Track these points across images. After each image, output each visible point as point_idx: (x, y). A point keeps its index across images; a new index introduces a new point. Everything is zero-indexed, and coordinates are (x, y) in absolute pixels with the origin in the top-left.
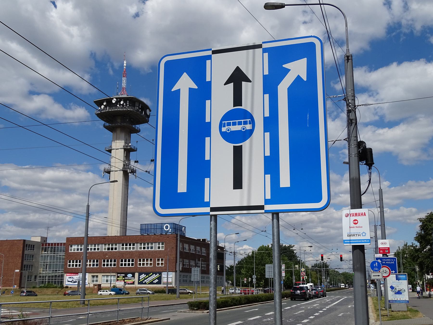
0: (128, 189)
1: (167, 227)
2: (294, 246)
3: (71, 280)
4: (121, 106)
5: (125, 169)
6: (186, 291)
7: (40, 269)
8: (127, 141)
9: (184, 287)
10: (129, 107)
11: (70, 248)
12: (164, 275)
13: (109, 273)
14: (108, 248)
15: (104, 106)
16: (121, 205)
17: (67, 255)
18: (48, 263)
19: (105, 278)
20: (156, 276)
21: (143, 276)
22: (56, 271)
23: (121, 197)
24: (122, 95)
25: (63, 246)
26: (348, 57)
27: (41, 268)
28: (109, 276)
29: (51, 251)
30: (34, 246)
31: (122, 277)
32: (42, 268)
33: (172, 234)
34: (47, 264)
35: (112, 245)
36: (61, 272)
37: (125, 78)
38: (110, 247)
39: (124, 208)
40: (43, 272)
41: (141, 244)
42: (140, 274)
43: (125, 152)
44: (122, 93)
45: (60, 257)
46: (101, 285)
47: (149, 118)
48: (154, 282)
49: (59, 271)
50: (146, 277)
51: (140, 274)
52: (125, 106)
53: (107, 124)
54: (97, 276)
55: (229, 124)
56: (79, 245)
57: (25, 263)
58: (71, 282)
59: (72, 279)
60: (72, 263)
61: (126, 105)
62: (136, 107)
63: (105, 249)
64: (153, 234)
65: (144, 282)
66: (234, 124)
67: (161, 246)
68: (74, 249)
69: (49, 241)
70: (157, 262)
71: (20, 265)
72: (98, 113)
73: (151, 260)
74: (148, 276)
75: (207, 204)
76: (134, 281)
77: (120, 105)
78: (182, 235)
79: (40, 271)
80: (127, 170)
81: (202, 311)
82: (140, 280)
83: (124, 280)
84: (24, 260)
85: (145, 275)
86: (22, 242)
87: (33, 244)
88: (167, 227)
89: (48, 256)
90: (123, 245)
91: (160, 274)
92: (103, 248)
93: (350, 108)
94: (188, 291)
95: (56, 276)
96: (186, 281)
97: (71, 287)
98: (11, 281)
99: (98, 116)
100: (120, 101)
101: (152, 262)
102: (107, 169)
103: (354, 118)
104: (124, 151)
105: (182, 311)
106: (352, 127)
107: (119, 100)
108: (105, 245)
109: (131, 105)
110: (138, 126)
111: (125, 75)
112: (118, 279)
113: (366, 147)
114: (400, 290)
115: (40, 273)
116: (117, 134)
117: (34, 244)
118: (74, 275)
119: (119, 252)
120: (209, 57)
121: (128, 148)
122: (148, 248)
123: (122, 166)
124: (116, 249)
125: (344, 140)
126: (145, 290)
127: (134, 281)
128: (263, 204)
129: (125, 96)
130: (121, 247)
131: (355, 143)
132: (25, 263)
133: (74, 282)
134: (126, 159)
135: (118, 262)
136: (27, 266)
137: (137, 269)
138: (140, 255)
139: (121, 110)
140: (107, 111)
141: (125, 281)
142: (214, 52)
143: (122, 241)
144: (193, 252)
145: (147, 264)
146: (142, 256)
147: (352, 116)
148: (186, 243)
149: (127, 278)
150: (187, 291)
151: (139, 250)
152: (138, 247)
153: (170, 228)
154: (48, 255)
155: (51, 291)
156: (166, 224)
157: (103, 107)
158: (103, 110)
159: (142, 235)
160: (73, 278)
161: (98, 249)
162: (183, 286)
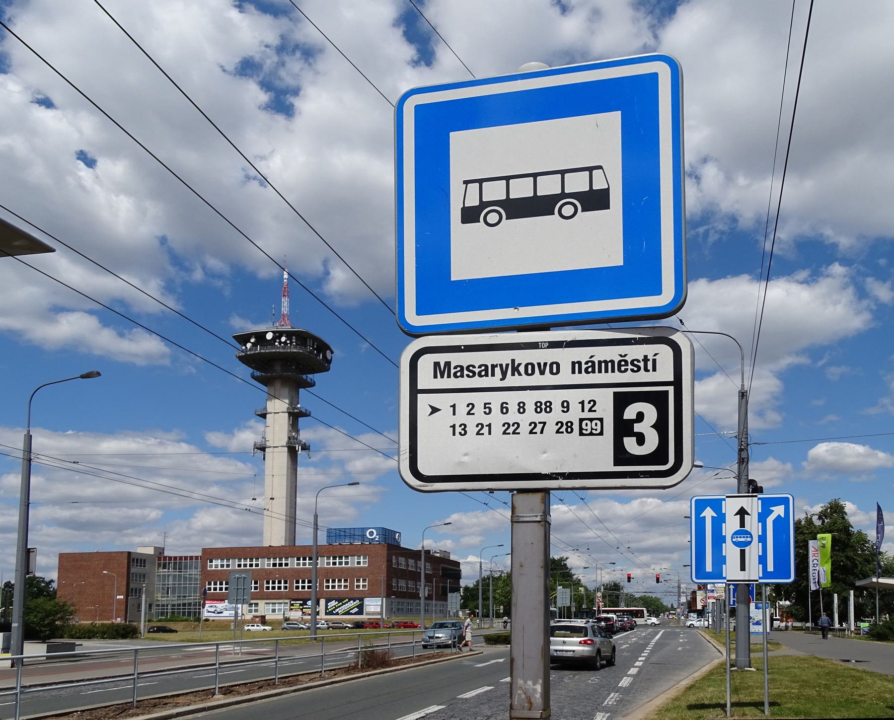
0: (296, 474)
1: (371, 534)
2: (567, 558)
3: (212, 609)
4: (282, 345)
5: (291, 444)
6: (341, 625)
7: (157, 594)
8: (293, 402)
9: (398, 618)
10: (295, 347)
11: (209, 564)
12: (367, 601)
13: (282, 599)
14: (273, 563)
15: (251, 344)
16: (24, 443)
17: (204, 573)
18: (170, 586)
19: (271, 607)
20: (355, 603)
21: (333, 603)
22: (185, 597)
23: (285, 488)
24: (283, 327)
25: (194, 561)
26: (743, 393)
27: (159, 593)
28: (277, 604)
29: (175, 568)
30: (145, 561)
31: (298, 605)
32: (160, 592)
33: (380, 543)
34: (168, 588)
35: (281, 559)
36: (193, 599)
37: (287, 299)
38: (278, 562)
39: (290, 504)
40: (162, 599)
41: (328, 558)
42: (328, 601)
43: (291, 417)
44: (283, 323)
45: (190, 576)
46: (264, 616)
47: (331, 365)
48: (351, 612)
49: (189, 596)
50: (339, 605)
51: (328, 601)
52: (289, 345)
53: (258, 374)
54: (256, 604)
55: (737, 537)
56: (224, 560)
57: (132, 586)
58: (214, 612)
59: (215, 609)
60: (214, 585)
61: (291, 343)
62: (308, 347)
63: (269, 565)
64: (349, 543)
65: (334, 612)
66: (740, 537)
67: (362, 560)
68: (216, 566)
69: (166, 554)
70: (356, 584)
71: (125, 588)
72: (241, 354)
73: (346, 581)
74: (341, 604)
75: (725, 578)
76: (319, 611)
77: (280, 343)
78: (395, 544)
79: (157, 597)
80: (294, 445)
81: (505, 646)
82: (328, 609)
83: (302, 609)
84: (131, 581)
85: (337, 602)
86: (126, 555)
87: (143, 558)
88: (371, 534)
89: (169, 575)
90: (298, 559)
91: (362, 600)
92: (266, 564)
93: (742, 447)
94: (345, 625)
95: (184, 605)
96: (411, 610)
97: (213, 620)
98: (111, 613)
99: (240, 360)
100: (280, 338)
101: (348, 584)
102: (259, 444)
103: (746, 456)
104: (289, 417)
105: (478, 645)
106: (744, 466)
107: (277, 335)
108: (269, 559)
109: (299, 343)
110: (310, 376)
111: (286, 294)
112: (292, 607)
113: (757, 485)
114: (759, 620)
115: (157, 600)
116: (275, 389)
117: (145, 558)
118: (218, 602)
119: (292, 570)
120: (724, 500)
121: (296, 411)
122: (341, 563)
123: (286, 439)
124: (286, 565)
125: (734, 478)
126: (296, 624)
127: (319, 611)
128: (758, 579)
129: (288, 328)
130: (296, 562)
131: (746, 481)
132: (132, 586)
133: (218, 613)
134: (292, 428)
135: (291, 584)
136: (136, 590)
137: (322, 594)
138: (327, 573)
139: (281, 350)
140: (257, 352)
141: (304, 611)
142: (727, 497)
143: (297, 553)
144: (404, 568)
145: (340, 586)
146: (331, 575)
147: (744, 455)
148: (402, 555)
149: (307, 607)
150: (299, 625)
151: (326, 566)
152: (323, 563)
153: (377, 535)
154: (169, 574)
155: (183, 626)
156: (370, 528)
157: (249, 345)
158: (250, 350)
159: (329, 545)
160: (216, 607)
161: (257, 565)
162: (398, 617)
